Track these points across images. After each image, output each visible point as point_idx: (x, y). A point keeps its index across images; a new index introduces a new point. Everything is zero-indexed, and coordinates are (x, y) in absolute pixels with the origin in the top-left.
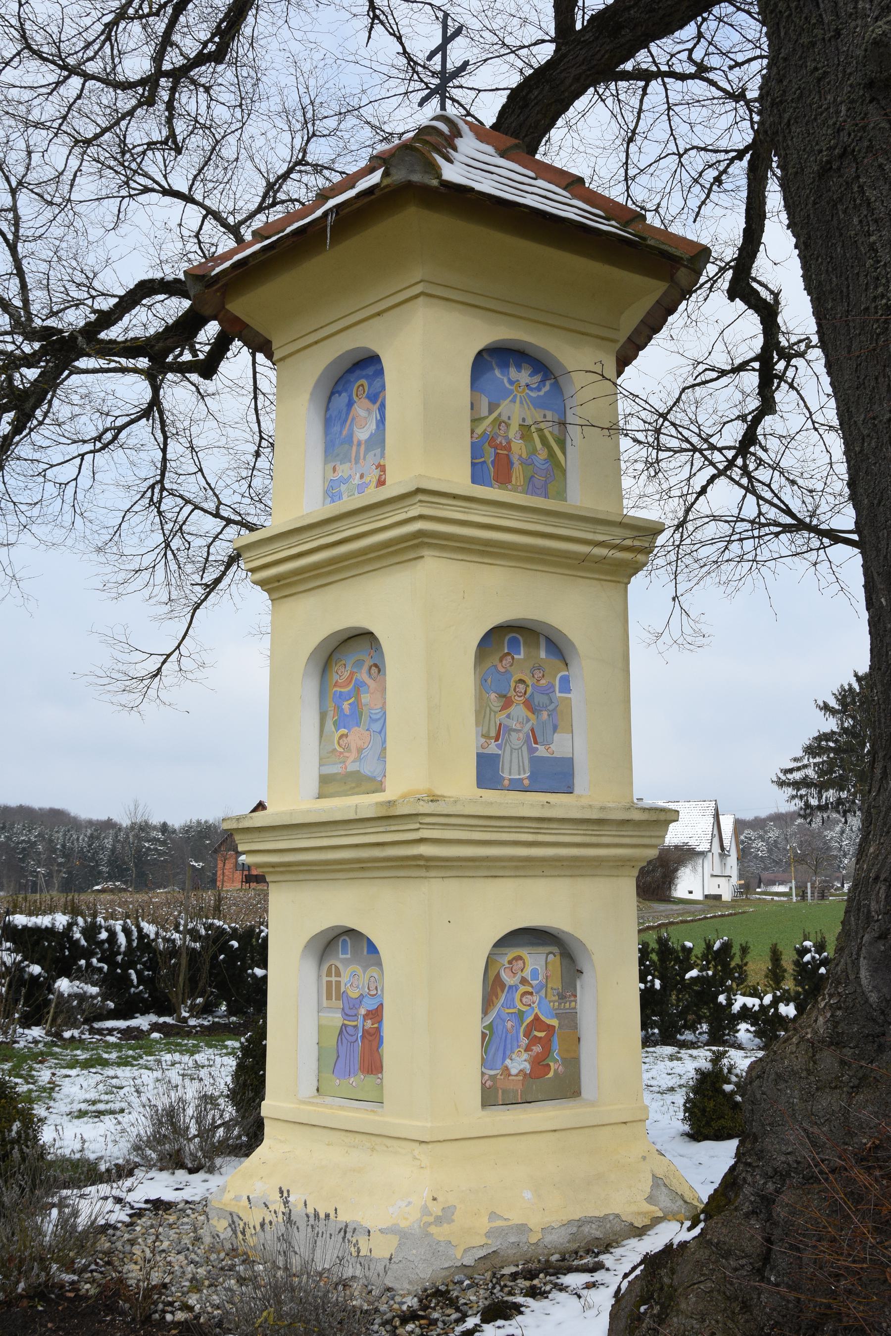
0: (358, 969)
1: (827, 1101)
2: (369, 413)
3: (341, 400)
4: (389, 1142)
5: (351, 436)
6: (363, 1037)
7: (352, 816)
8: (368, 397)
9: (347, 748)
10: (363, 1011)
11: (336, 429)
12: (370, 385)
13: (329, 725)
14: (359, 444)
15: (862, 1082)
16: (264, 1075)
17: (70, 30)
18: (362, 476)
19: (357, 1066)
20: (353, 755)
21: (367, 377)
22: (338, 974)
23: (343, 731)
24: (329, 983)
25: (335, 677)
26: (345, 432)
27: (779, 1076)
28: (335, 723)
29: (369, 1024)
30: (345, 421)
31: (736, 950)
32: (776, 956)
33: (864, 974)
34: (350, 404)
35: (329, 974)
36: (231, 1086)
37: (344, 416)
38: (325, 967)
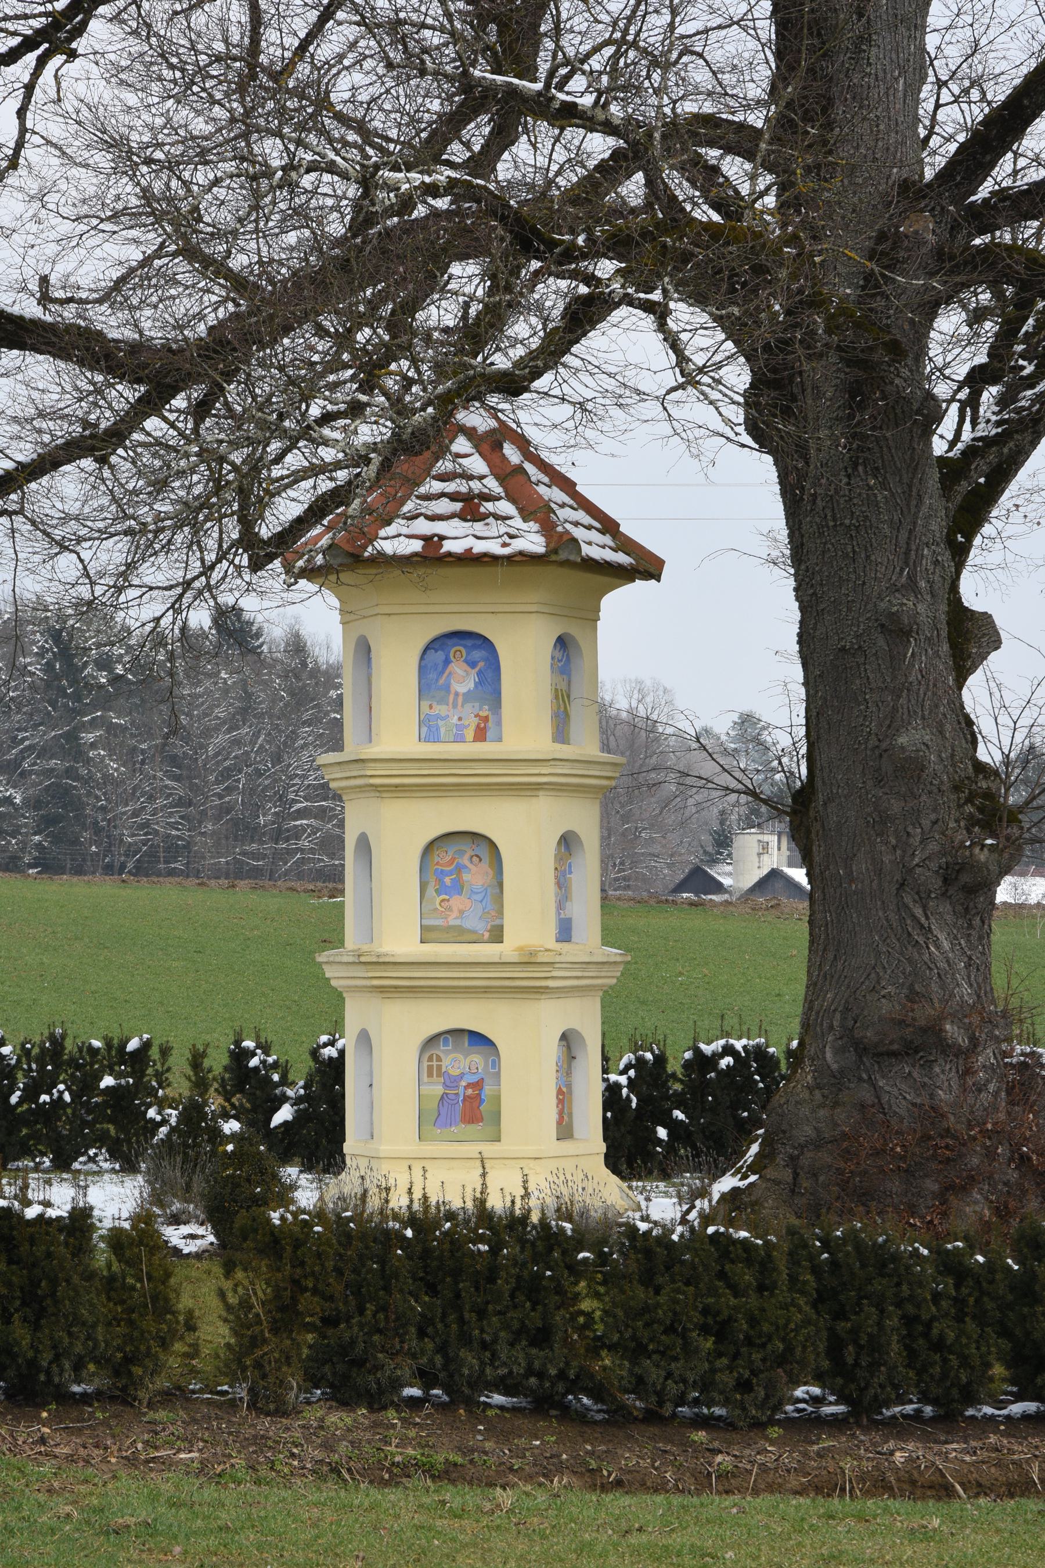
0: (461, 1057)
1: (822, 1113)
2: (468, 674)
3: (439, 656)
4: (507, 1162)
5: (447, 688)
6: (464, 1100)
7: (497, 960)
8: (466, 661)
9: (450, 909)
10: (463, 1083)
11: (433, 676)
12: (468, 654)
13: (431, 891)
14: (457, 694)
15: (836, 1104)
16: (605, 1110)
17: (94, 181)
18: (460, 719)
19: (458, 1119)
20: (455, 914)
21: (465, 646)
22: (439, 1059)
23: (444, 897)
24: (430, 1068)
25: (436, 859)
26: (442, 681)
27: (797, 1102)
28: (436, 891)
29: (470, 1091)
30: (443, 672)
31: (154, 1053)
32: (196, 1061)
33: (829, 1055)
34: (447, 662)
35: (430, 1059)
36: (117, 1167)
37: (440, 669)
38: (426, 1056)
